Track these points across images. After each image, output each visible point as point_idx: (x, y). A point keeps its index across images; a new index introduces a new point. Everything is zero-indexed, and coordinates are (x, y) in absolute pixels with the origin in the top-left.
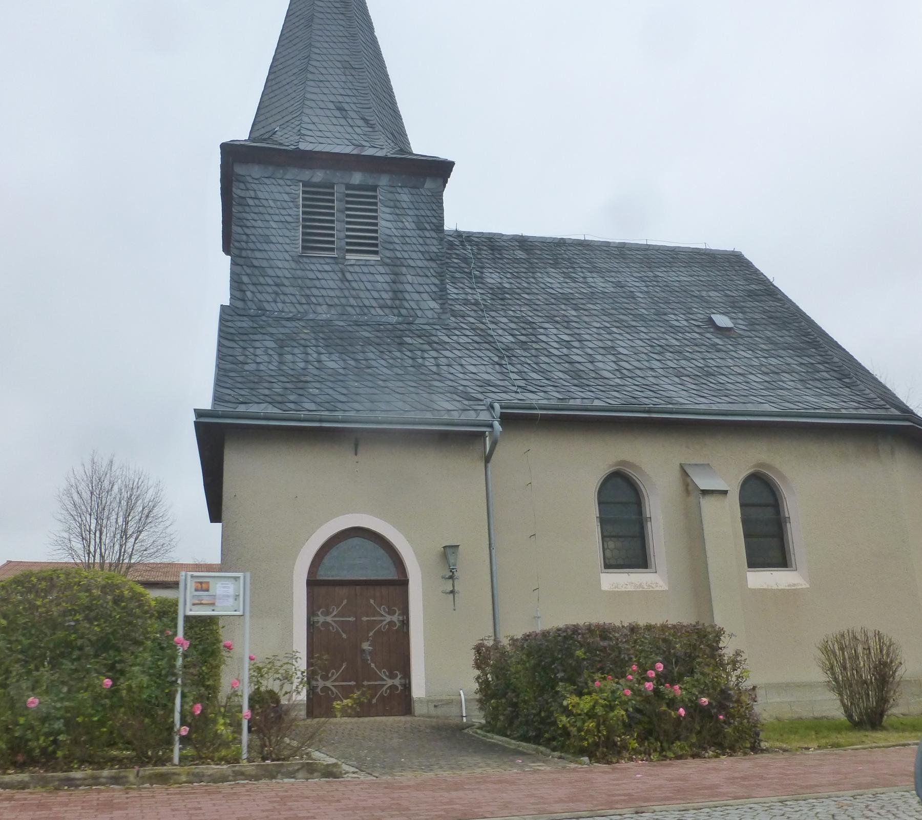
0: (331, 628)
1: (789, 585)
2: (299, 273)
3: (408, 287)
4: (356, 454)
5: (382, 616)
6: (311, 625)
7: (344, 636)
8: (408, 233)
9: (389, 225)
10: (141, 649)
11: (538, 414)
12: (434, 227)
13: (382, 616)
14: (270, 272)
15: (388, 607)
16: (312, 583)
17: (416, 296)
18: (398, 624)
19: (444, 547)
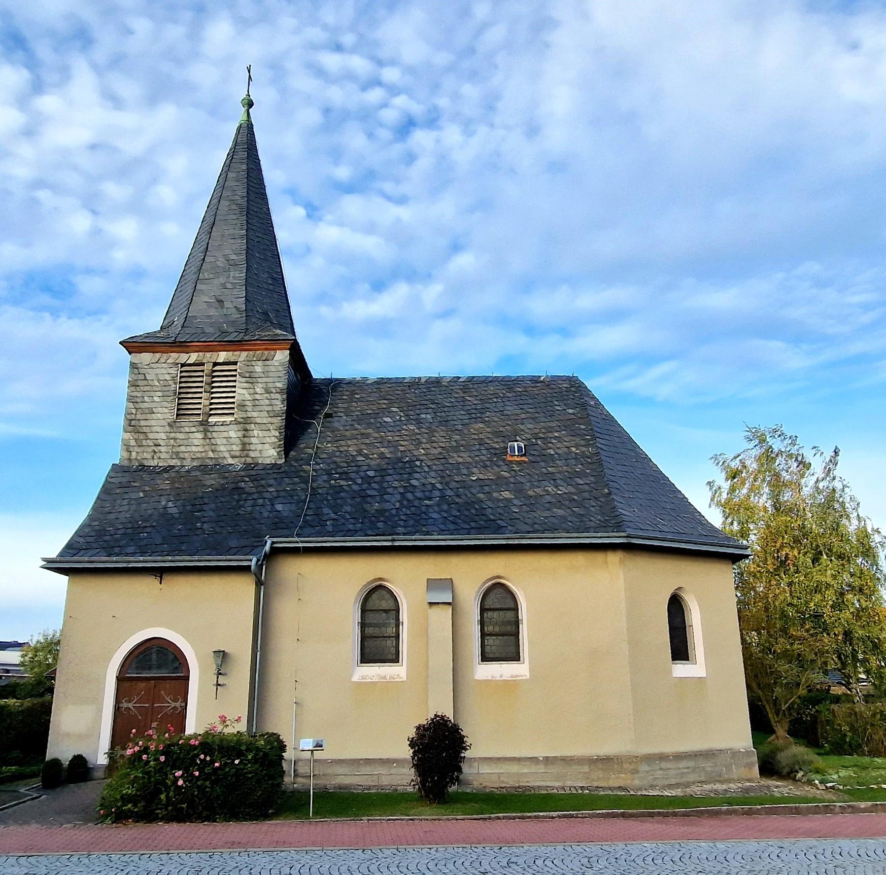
0: (172, 698)
1: (512, 677)
2: (172, 435)
3: (254, 440)
4: (161, 583)
5: (169, 703)
6: (117, 709)
7: (140, 718)
8: (258, 397)
9: (244, 391)
10: (738, 491)
11: (300, 547)
12: (279, 391)
13: (169, 703)
14: (151, 436)
15: (129, 713)
16: (120, 679)
17: (260, 447)
18: (180, 709)
19: (451, 579)
